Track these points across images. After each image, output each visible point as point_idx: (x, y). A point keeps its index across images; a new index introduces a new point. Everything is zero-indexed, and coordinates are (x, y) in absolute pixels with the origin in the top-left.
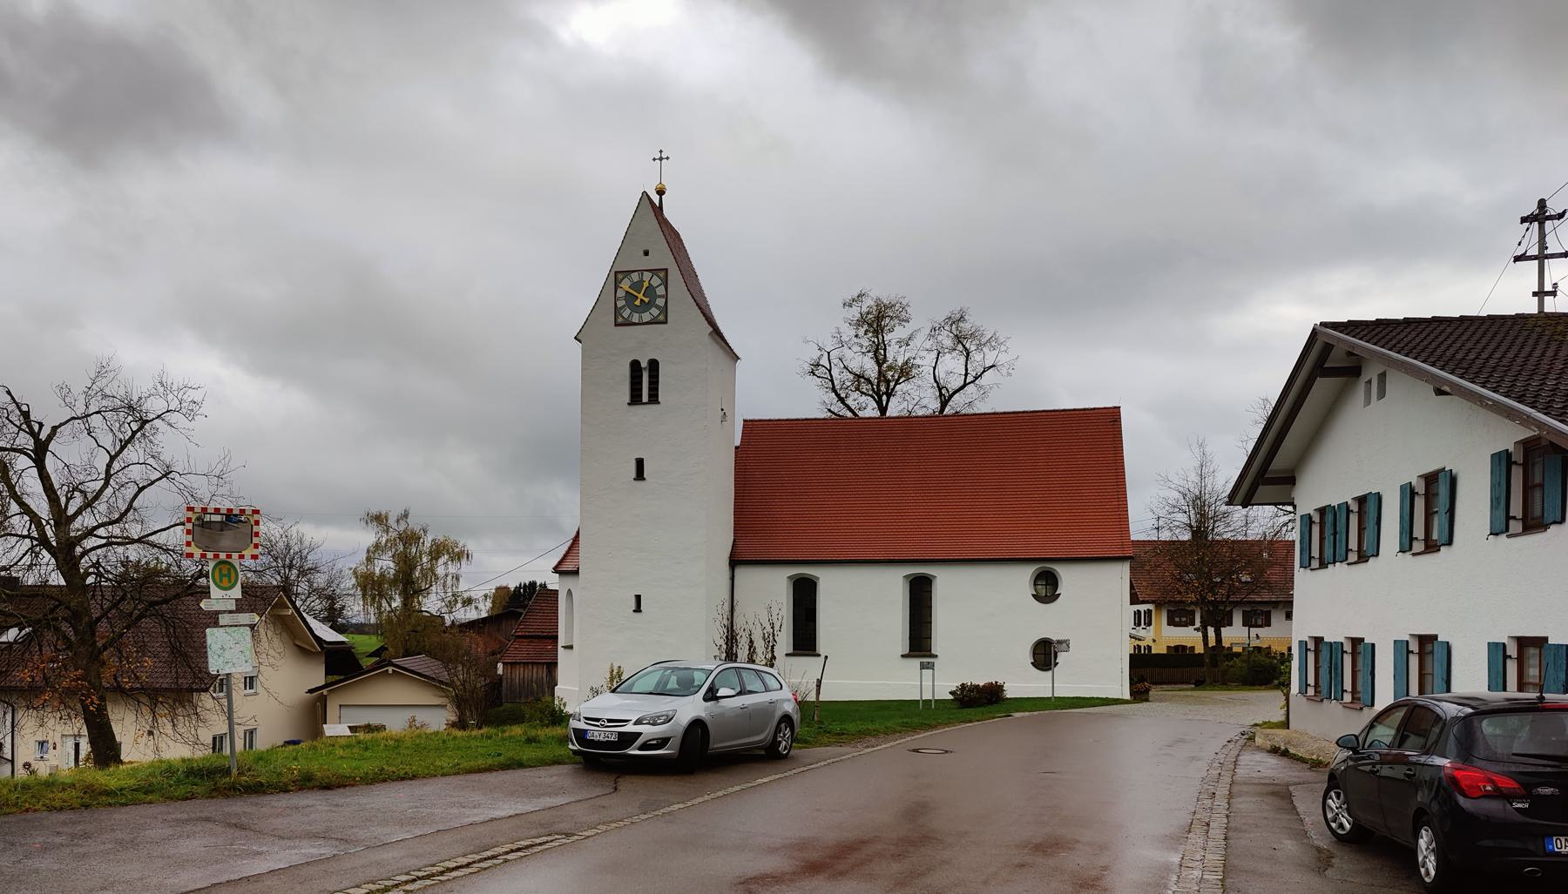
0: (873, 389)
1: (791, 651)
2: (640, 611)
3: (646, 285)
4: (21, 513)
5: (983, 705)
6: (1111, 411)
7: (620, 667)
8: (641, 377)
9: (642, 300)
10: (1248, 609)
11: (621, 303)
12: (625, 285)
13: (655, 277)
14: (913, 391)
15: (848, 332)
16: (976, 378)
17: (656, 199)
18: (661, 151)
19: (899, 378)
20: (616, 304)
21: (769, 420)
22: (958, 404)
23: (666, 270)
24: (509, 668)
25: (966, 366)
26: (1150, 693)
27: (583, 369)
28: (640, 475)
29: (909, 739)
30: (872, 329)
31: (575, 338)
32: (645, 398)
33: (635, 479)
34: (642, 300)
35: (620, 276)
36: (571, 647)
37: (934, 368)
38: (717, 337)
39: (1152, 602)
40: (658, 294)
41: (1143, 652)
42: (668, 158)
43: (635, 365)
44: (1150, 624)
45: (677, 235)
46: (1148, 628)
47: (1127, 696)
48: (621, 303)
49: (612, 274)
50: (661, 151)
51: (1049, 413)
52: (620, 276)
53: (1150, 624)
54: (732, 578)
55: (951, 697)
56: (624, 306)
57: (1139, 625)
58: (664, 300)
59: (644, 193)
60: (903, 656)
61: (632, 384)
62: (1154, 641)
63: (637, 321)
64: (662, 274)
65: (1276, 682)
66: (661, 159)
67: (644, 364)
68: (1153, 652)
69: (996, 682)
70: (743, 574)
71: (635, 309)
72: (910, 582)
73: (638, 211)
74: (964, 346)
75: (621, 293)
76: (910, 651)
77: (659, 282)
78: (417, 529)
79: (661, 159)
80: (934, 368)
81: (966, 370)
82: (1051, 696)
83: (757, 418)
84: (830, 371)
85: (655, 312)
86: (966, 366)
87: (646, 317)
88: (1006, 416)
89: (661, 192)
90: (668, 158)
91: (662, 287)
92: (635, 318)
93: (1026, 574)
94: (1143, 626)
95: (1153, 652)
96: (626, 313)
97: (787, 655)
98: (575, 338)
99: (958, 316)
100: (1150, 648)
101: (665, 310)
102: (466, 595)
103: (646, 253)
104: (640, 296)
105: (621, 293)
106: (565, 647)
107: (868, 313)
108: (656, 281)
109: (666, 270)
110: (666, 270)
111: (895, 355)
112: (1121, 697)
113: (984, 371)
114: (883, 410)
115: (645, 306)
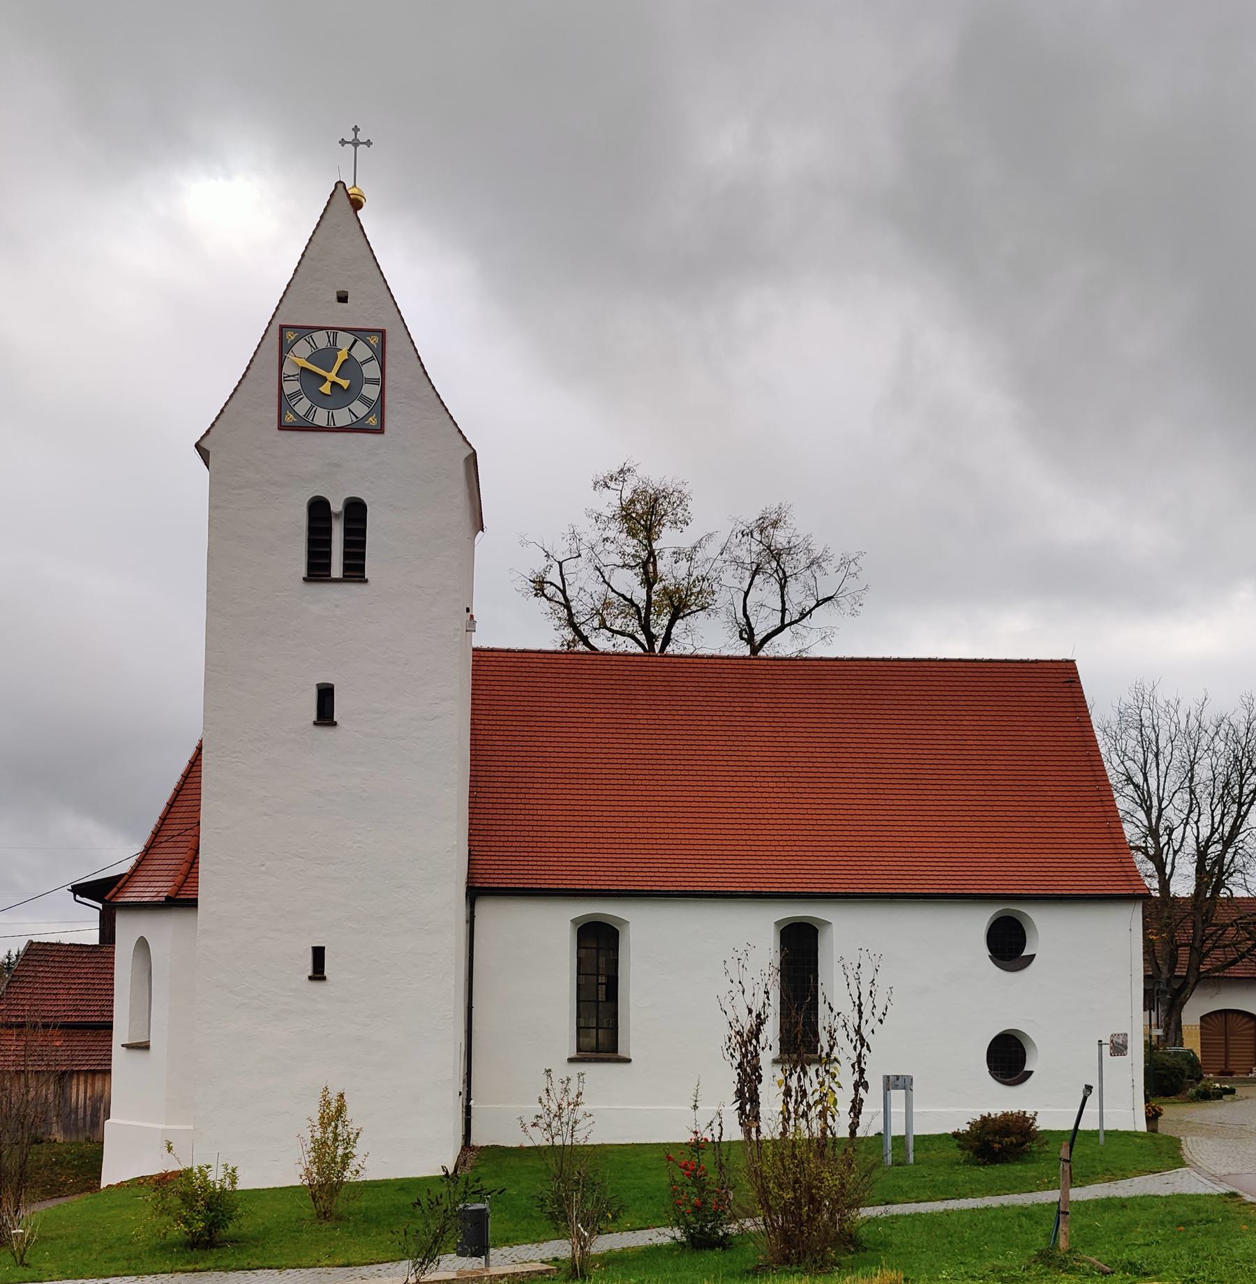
1: (574, 1054)
2: (324, 979)
3: (342, 356)
7: (342, 1096)
8: (329, 531)
9: (333, 383)
11: (291, 387)
12: (300, 355)
13: (359, 343)
18: (343, 142)
20: (281, 388)
21: (508, 651)
23: (382, 333)
27: (213, 507)
32: (337, 570)
33: (315, 724)
35: (290, 336)
36: (145, 1047)
37: (746, 594)
43: (318, 510)
48: (291, 387)
49: (275, 328)
50: (356, 129)
54: (471, 921)
56: (297, 393)
59: (340, 183)
60: (571, 1060)
61: (312, 542)
63: (324, 424)
64: (374, 340)
65: (1192, 1091)
66: (356, 143)
67: (337, 506)
69: (990, 1115)
70: (488, 911)
71: (320, 400)
73: (327, 216)
82: (1096, 1127)
84: (563, 592)
85: (360, 409)
87: (342, 417)
91: (375, 364)
92: (321, 418)
93: (979, 920)
96: (302, 406)
101: (379, 407)
103: (343, 298)
104: (332, 376)
106: (129, 1047)
107: (632, 502)
109: (383, 332)
110: (382, 333)
111: (670, 570)
115: (341, 396)
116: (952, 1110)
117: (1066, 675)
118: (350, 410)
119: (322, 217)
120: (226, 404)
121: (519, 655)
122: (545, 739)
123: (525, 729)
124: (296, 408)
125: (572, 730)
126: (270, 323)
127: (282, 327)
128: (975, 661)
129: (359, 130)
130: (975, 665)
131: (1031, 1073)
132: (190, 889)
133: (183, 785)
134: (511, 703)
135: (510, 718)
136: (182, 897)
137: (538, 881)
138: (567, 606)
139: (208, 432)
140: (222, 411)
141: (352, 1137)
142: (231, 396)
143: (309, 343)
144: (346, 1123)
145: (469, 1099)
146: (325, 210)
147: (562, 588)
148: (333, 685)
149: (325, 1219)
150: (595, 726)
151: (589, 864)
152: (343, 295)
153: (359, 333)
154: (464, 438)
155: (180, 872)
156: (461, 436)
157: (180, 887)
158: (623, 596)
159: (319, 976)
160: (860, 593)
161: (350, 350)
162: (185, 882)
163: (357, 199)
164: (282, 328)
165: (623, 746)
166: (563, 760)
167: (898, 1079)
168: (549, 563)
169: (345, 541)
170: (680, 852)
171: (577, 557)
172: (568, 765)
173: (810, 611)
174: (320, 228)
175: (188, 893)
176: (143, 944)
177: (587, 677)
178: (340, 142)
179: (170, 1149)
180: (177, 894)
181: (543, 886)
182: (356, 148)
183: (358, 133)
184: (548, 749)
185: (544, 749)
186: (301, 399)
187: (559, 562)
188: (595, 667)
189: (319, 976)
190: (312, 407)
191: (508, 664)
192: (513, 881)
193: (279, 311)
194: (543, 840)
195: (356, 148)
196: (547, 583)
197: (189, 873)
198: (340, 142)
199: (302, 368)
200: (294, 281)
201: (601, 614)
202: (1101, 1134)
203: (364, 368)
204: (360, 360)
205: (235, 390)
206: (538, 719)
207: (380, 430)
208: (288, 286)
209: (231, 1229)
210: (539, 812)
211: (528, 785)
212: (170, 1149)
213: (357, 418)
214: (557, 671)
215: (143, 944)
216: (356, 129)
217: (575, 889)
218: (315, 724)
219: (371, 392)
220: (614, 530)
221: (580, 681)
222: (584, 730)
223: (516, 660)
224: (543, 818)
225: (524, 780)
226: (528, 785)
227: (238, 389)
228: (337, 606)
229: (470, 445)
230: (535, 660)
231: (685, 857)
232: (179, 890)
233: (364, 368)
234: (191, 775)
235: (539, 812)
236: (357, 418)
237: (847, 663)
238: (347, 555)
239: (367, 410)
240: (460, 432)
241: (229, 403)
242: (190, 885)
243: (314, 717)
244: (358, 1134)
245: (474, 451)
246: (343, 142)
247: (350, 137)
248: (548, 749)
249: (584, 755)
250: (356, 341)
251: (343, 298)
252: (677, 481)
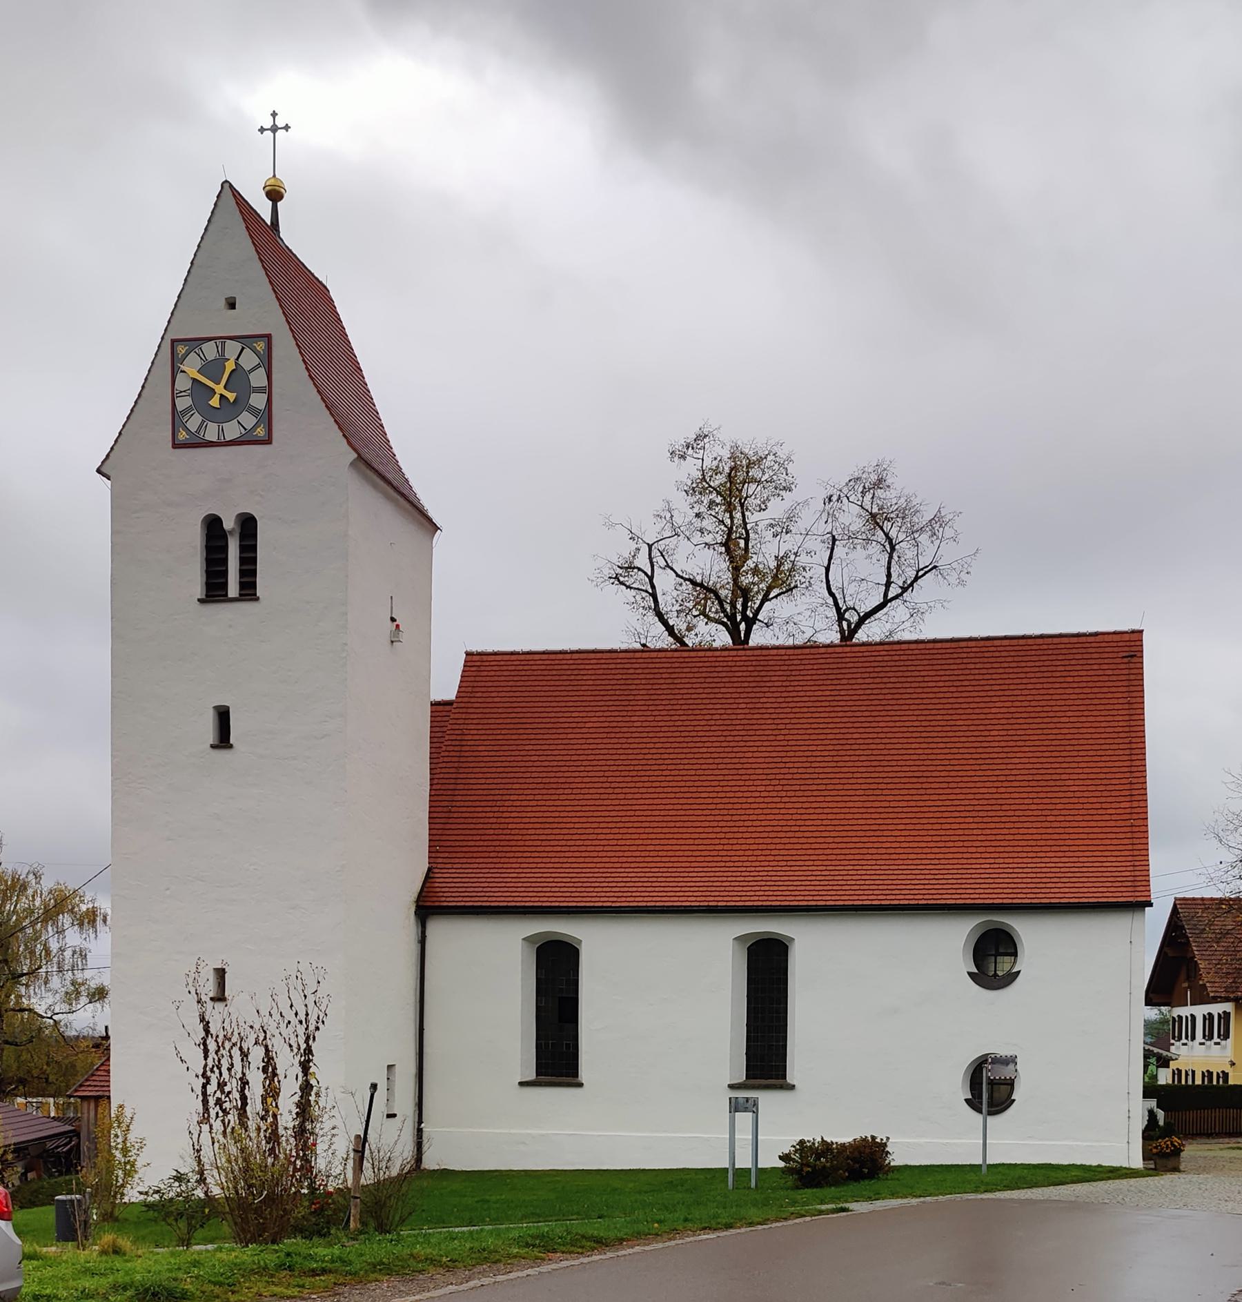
0: (724, 611)
1: (531, 1075)
3: (230, 366)
5: (836, 1183)
6: (1126, 637)
8: (225, 549)
9: (222, 396)
10: (746, 646)
12: (191, 367)
13: (247, 350)
14: (800, 618)
15: (684, 509)
16: (904, 590)
17: (263, 208)
18: (274, 114)
19: (770, 589)
22: (870, 632)
23: (268, 337)
24: (92, 1105)
25: (889, 568)
26: (1182, 1154)
28: (223, 739)
29: (660, 1245)
31: (99, 471)
32: (233, 590)
33: (212, 746)
34: (222, 396)
35: (181, 350)
37: (827, 569)
38: (369, 472)
39: (1227, 1000)
41: (1215, 1083)
42: (287, 128)
43: (213, 525)
44: (1226, 1036)
45: (320, 292)
46: (1223, 1043)
47: (1137, 1162)
48: (183, 403)
50: (274, 114)
51: (1015, 642)
52: (181, 350)
53: (1226, 1036)
54: (422, 941)
55: (782, 1164)
56: (189, 409)
57: (1211, 1038)
58: (265, 396)
62: (1233, 1064)
64: (261, 346)
66: (274, 129)
67: (229, 524)
68: (1231, 1082)
70: (439, 929)
71: (210, 415)
72: (748, 949)
74: (887, 535)
75: (183, 384)
76: (748, 1077)
78: (23, 872)
79: (274, 129)
80: (827, 569)
81: (889, 575)
83: (490, 650)
84: (651, 578)
85: (248, 420)
86: (889, 568)
87: (232, 431)
88: (939, 645)
89: (275, 195)
90: (287, 128)
91: (262, 372)
92: (211, 434)
94: (1216, 1039)
95: (1231, 1082)
96: (194, 422)
97: (521, 1084)
98: (99, 471)
99: (874, 478)
100: (1226, 1075)
101: (267, 416)
102: (93, 984)
103: (232, 305)
104: (220, 389)
105: (183, 384)
107: (716, 471)
108: (249, 360)
109: (269, 337)
110: (268, 337)
111: (765, 552)
112: (1125, 1165)
113: (917, 578)
114: (740, 640)
115: (230, 410)
116: (923, 1140)
117: (1127, 649)
118: (239, 422)
119: (209, 221)
123: (513, 737)
127: (173, 341)
128: (1023, 637)
129: (277, 114)
130: (1022, 642)
131: (1014, 1100)
139: (108, 456)
143: (199, 355)
145: (420, 1122)
147: (650, 574)
148: (228, 707)
151: (1053, 870)
153: (246, 340)
160: (969, 559)
161: (237, 359)
163: (275, 190)
167: (747, 1101)
170: (1020, 860)
173: (912, 585)
174: (209, 233)
178: (259, 130)
186: (192, 415)
190: (203, 422)
191: (510, 668)
192: (888, 897)
196: (634, 568)
198: (259, 130)
199: (194, 380)
200: (184, 292)
202: (984, 1169)
204: (247, 368)
207: (268, 441)
208: (179, 297)
213: (245, 429)
214: (559, 672)
219: (258, 401)
228: (230, 626)
231: (1025, 866)
236: (245, 429)
237: (874, 648)
239: (254, 420)
247: (268, 123)
250: (243, 349)
252: (772, 442)
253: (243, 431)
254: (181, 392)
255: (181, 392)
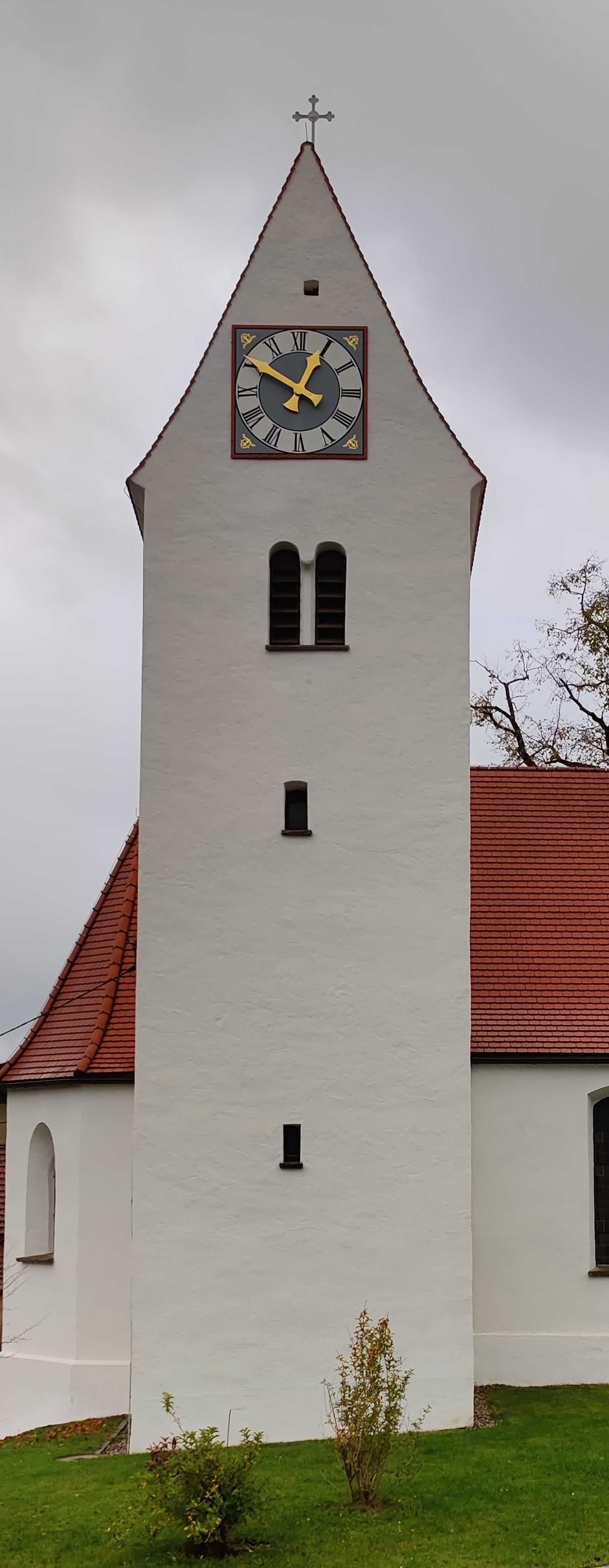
2: (300, 1166)
3: (313, 362)
4: (221, 1444)
7: (385, 1323)
8: (296, 587)
9: (302, 397)
13: (335, 345)
20: (235, 406)
23: (363, 332)
30: (390, 1384)
32: (307, 636)
35: (246, 339)
36: (47, 1260)
40: (341, 407)
56: (255, 412)
58: (358, 402)
63: (290, 450)
64: (353, 341)
66: (314, 117)
67: (307, 555)
71: (283, 419)
75: (247, 379)
77: (347, 358)
84: (512, 718)
87: (314, 441)
91: (354, 371)
92: (286, 442)
96: (262, 428)
103: (312, 290)
104: (300, 388)
105: (247, 379)
108: (337, 356)
110: (363, 332)
118: (323, 431)
120: (165, 428)
121: (493, 774)
122: (534, 872)
124: (254, 431)
125: (567, 861)
126: (220, 324)
129: (317, 100)
132: (103, 1061)
133: (86, 938)
134: (488, 830)
135: (488, 848)
136: (95, 1071)
137: (546, 1045)
138: (517, 733)
139: (142, 464)
140: (160, 437)
141: (398, 1382)
142: (171, 418)
143: (270, 347)
144: (392, 1363)
146: (289, 179)
147: (510, 714)
148: (306, 784)
149: (367, 1503)
150: (596, 855)
152: (311, 287)
154: (471, 462)
155: (90, 1042)
156: (467, 460)
157: (92, 1059)
158: (593, 715)
159: (293, 1163)
161: (322, 354)
162: (97, 1053)
164: (236, 329)
165: (503, 935)
166: (560, 897)
168: (494, 685)
169: (317, 599)
171: (524, 679)
172: (566, 903)
174: (282, 202)
175: (102, 1066)
176: (43, 1133)
177: (579, 797)
179: (168, 1404)
180: (89, 1068)
181: (553, 1051)
182: (313, 122)
183: (317, 104)
184: (540, 884)
185: (535, 884)
186: (260, 418)
187: (504, 684)
188: (587, 786)
189: (293, 1163)
190: (274, 429)
193: (231, 309)
194: (544, 994)
195: (313, 122)
197: (102, 1042)
201: (552, 748)
203: (340, 376)
204: (335, 366)
205: (177, 409)
206: (523, 848)
207: (361, 456)
208: (243, 276)
209: (250, 1523)
210: (536, 961)
211: (519, 928)
212: (168, 1404)
213: (332, 440)
215: (43, 1133)
216: (314, 100)
217: (594, 1054)
218: (284, 834)
220: (569, 645)
221: (571, 803)
222: (582, 861)
223: (490, 779)
224: (542, 967)
225: (512, 922)
226: (519, 928)
227: (181, 408)
228: (309, 682)
229: (478, 470)
230: (513, 779)
232: (91, 1063)
233: (340, 376)
234: (96, 925)
235: (536, 961)
236: (332, 440)
238: (320, 618)
239: (344, 430)
240: (465, 453)
241: (170, 427)
242: (104, 1056)
243: (282, 826)
244: (406, 1378)
245: (484, 478)
246: (298, 116)
247: (306, 109)
248: (540, 884)
249: (585, 891)
250: (329, 342)
251: (312, 290)
253: (329, 442)
254: (245, 390)
255: (245, 390)
